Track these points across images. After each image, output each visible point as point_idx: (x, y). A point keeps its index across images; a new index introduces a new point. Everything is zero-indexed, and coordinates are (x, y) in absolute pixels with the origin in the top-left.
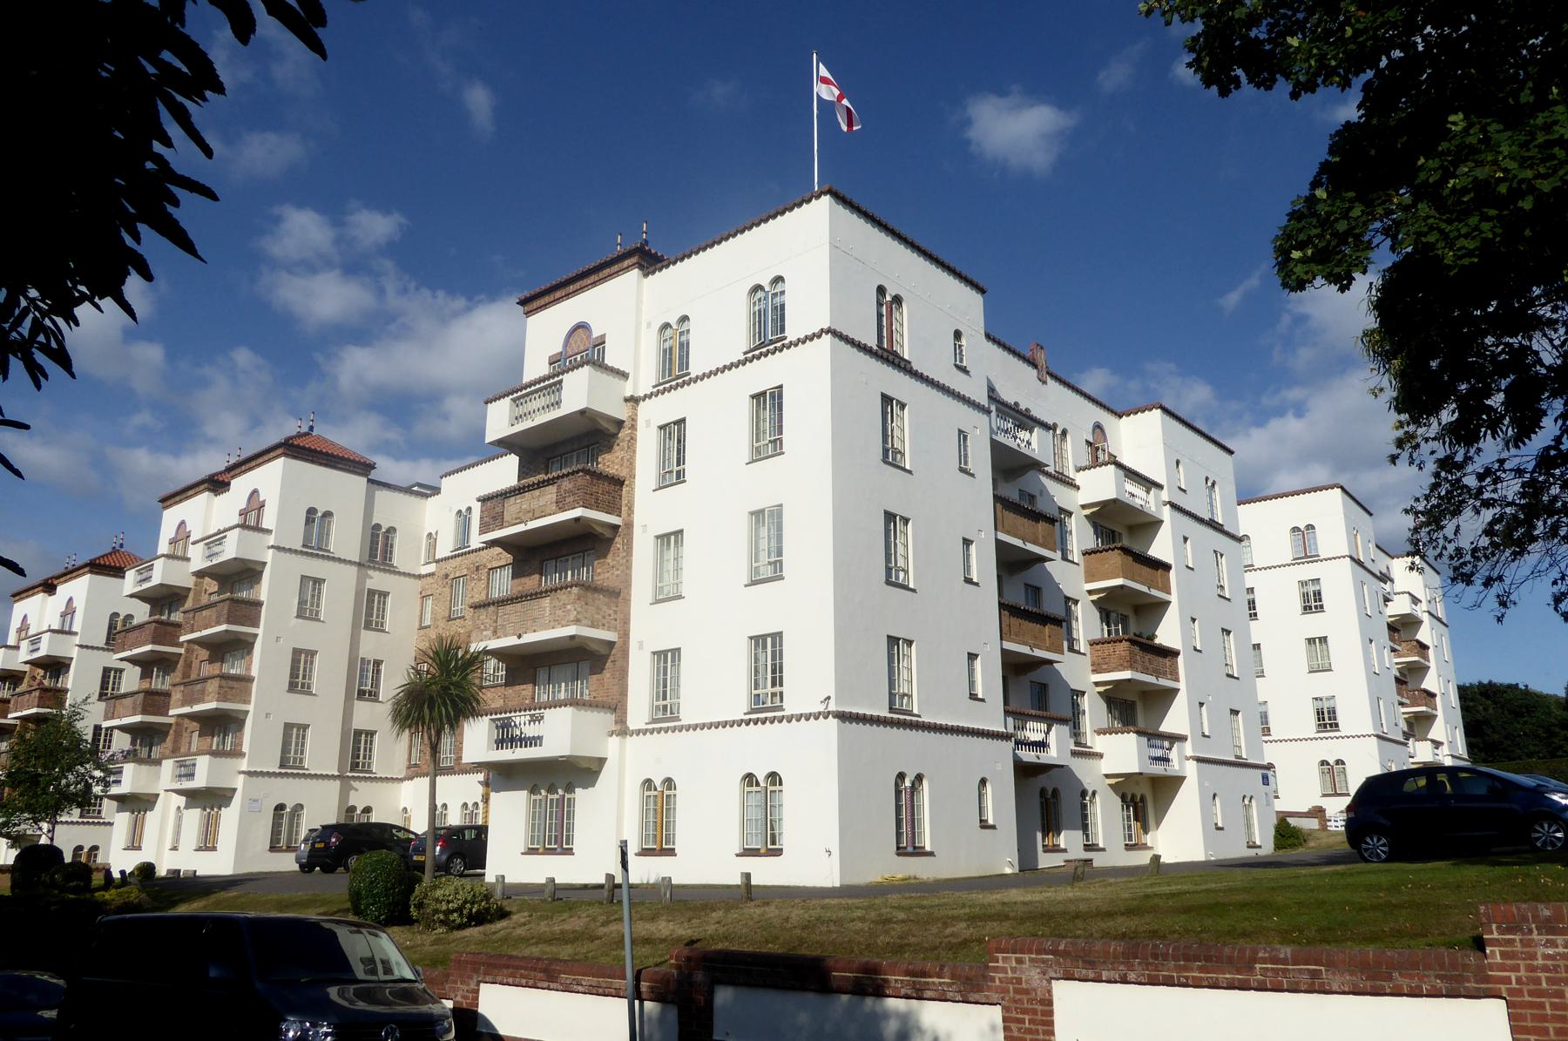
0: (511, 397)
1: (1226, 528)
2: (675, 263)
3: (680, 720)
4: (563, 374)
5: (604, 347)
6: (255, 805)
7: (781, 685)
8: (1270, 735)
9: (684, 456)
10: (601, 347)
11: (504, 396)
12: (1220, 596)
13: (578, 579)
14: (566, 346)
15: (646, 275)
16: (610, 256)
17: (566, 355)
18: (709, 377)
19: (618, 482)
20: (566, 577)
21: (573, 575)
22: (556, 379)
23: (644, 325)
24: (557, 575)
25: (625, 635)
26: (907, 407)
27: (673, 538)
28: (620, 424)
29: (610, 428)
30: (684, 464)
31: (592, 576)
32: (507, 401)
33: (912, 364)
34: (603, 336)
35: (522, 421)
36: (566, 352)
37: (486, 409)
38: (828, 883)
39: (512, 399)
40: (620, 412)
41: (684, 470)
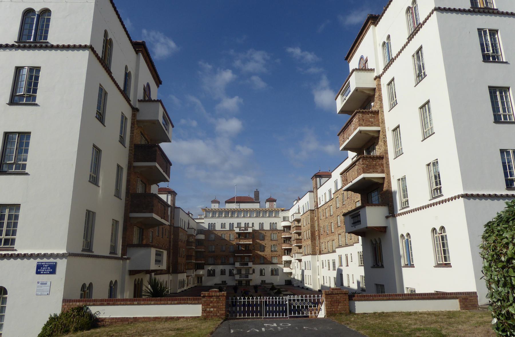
1: (501, 10)
2: (382, 15)
3: (226, 228)
6: (44, 287)
7: (440, 184)
8: (442, 195)
12: (158, 82)
15: (376, 26)
18: (399, 55)
19: (376, 113)
23: (378, 46)
25: (388, 174)
26: (499, 30)
28: (374, 89)
33: (499, 10)
37: (336, 101)
38: (357, 302)
40: (372, 84)
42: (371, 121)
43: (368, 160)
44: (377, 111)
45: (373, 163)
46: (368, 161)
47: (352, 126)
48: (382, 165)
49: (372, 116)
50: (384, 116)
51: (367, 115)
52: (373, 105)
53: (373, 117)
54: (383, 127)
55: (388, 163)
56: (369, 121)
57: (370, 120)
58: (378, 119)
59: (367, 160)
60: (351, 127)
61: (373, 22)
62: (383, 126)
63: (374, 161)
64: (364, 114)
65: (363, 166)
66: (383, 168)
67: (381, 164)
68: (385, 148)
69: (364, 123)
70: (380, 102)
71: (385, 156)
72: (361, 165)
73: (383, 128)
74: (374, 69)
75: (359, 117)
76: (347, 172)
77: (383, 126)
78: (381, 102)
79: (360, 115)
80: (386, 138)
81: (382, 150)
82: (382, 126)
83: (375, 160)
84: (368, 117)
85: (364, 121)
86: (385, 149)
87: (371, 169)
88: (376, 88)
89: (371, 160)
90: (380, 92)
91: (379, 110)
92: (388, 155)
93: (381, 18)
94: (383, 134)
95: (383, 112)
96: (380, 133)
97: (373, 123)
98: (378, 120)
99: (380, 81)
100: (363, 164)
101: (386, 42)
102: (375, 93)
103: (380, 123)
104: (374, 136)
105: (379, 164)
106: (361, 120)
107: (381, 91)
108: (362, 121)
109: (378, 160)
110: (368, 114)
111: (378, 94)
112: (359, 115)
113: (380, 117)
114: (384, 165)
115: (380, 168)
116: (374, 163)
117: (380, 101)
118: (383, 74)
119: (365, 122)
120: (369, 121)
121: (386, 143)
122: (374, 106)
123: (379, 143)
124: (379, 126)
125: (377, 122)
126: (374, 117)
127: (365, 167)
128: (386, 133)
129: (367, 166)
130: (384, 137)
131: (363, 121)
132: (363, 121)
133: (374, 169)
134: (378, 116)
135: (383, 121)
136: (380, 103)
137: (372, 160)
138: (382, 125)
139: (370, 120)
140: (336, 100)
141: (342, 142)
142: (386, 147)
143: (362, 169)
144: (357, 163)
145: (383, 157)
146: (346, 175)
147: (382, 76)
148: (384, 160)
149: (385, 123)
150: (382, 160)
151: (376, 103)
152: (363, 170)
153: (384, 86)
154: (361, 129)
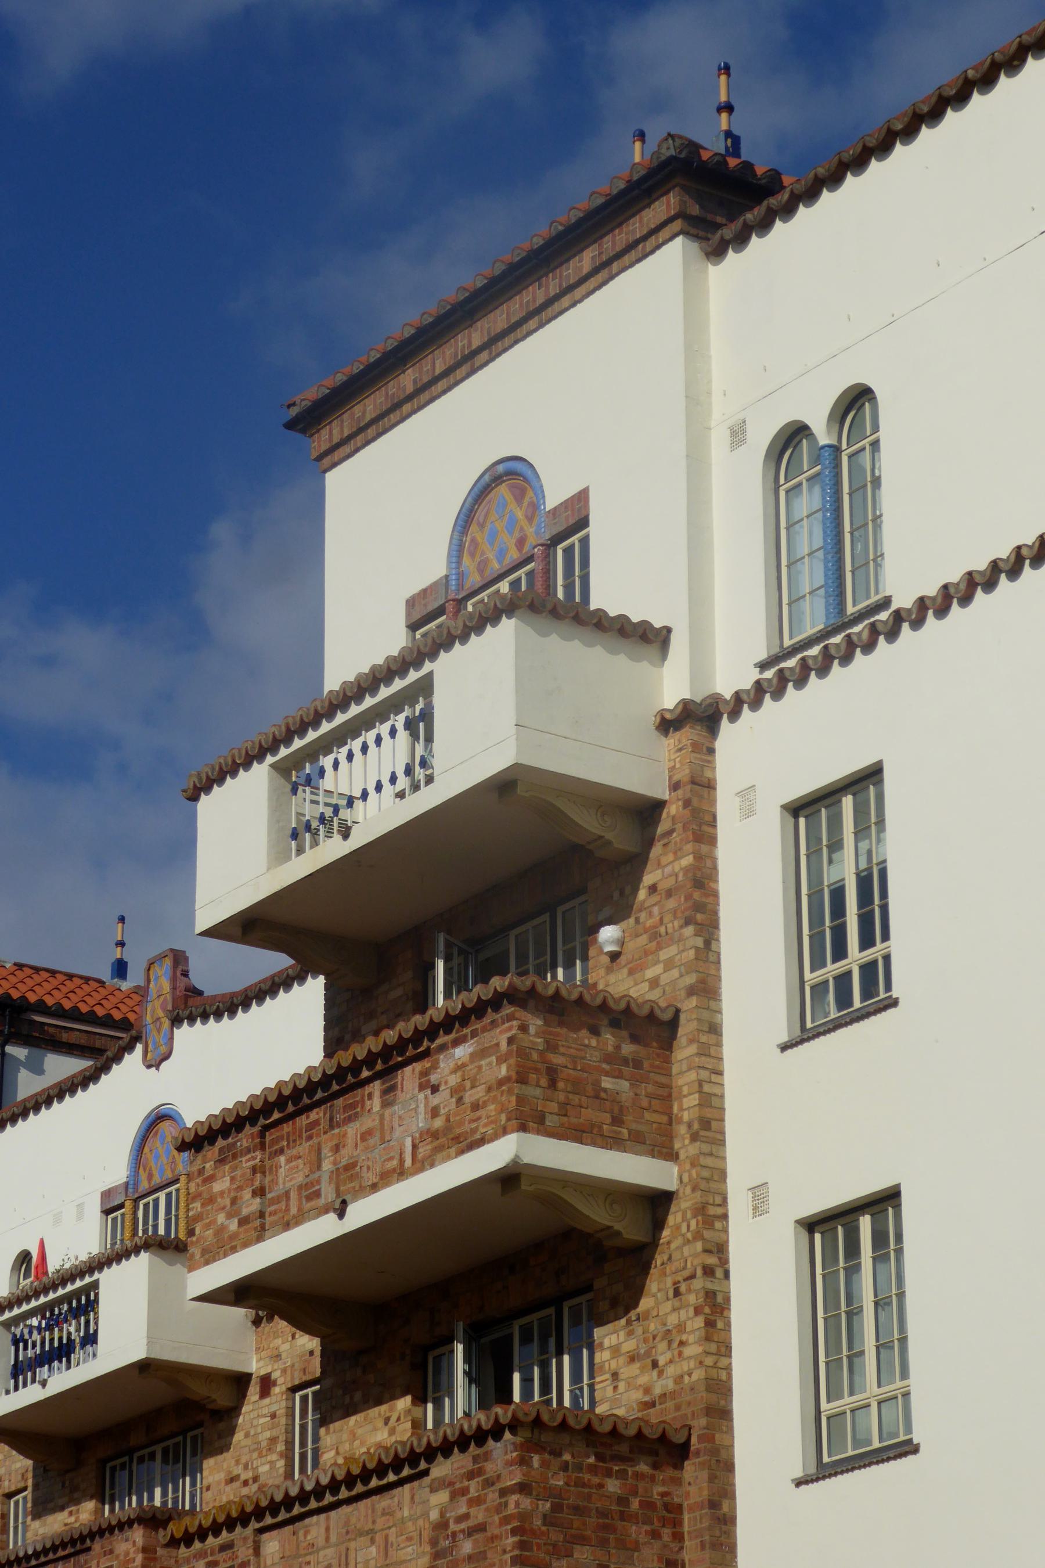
0: (270, 759)
2: (811, 195)
4: (433, 655)
5: (585, 542)
9: (884, 909)
10: (575, 539)
11: (248, 761)
13: (175, 1500)
14: (460, 557)
15: (717, 253)
16: (364, 359)
17: (460, 586)
18: (966, 600)
20: (151, 1498)
21: (164, 1494)
22: (413, 676)
23: (718, 439)
24: (188, 1479)
27: (865, 1223)
29: (609, 836)
30: (886, 937)
31: (591, 1387)
32: (259, 775)
34: (583, 496)
35: (315, 843)
36: (461, 576)
39: (272, 766)
41: (887, 959)
42: (614, 1098)
43: (567, 1457)
44: (667, 1016)
45: (601, 1486)
46: (565, 1467)
47: (401, 1096)
48: (673, 1513)
49: (618, 1048)
50: (720, 1073)
51: (584, 1033)
52: (609, 948)
53: (625, 1061)
54: (706, 1173)
55: (725, 1507)
56: (598, 1093)
57: (607, 1083)
58: (663, 1092)
59: (557, 1453)
60: (385, 1104)
61: (695, 210)
62: (709, 1161)
63: (609, 1474)
64: (561, 1024)
65: (526, 1503)
66: (674, 1546)
67: (667, 1507)
68: (709, 1361)
69: (554, 1107)
70: (699, 942)
71: (708, 1438)
72: (504, 1492)
73: (708, 1180)
74: (669, 630)
75: (526, 1040)
76: (261, 1531)
77: (709, 1161)
78: (708, 943)
79: (535, 1023)
80: (727, 1275)
81: (671, 1371)
82: (703, 1161)
83: (623, 1459)
84: (593, 1057)
85: (561, 1085)
86: (713, 1373)
87: (583, 1540)
88: (673, 809)
89: (592, 1460)
90: (704, 848)
91: (678, 1011)
92: (730, 1430)
93: (788, 211)
94: (707, 1234)
95: (710, 1039)
96: (671, 1220)
97: (628, 1118)
98: (666, 1097)
99: (711, 751)
100: (523, 1488)
101: (823, 437)
102: (649, 843)
103: (683, 1130)
104: (618, 1233)
105: (648, 1505)
106: (533, 1077)
107: (713, 841)
108: (544, 1082)
109: (643, 1468)
110: (595, 1031)
111: (687, 861)
112: (523, 1028)
113: (692, 1076)
114: (686, 1517)
115: (657, 1545)
116: (613, 1486)
117: (697, 934)
118: (756, 704)
119: (562, 1097)
120: (597, 1097)
121: (720, 1325)
122: (614, 956)
123: (645, 1303)
124: (671, 1156)
125: (656, 1117)
126: (637, 1064)
127: (538, 1522)
128: (726, 1231)
129: (556, 1508)
130: (712, 1260)
131: (553, 1084)
132: (553, 1084)
133: (603, 1543)
134: (668, 1060)
135: (708, 1113)
136: (697, 949)
137: (600, 1457)
138: (706, 1148)
139: (607, 1083)
140: (194, 798)
141: (233, 1225)
142: (723, 1362)
143: (514, 1532)
144: (441, 1469)
145: (687, 1444)
146: (257, 1550)
147: (735, 715)
148: (690, 1469)
149: (722, 1133)
150: (670, 1472)
151: (655, 936)
152: (522, 1545)
153: (748, 812)
154: (526, 1159)
